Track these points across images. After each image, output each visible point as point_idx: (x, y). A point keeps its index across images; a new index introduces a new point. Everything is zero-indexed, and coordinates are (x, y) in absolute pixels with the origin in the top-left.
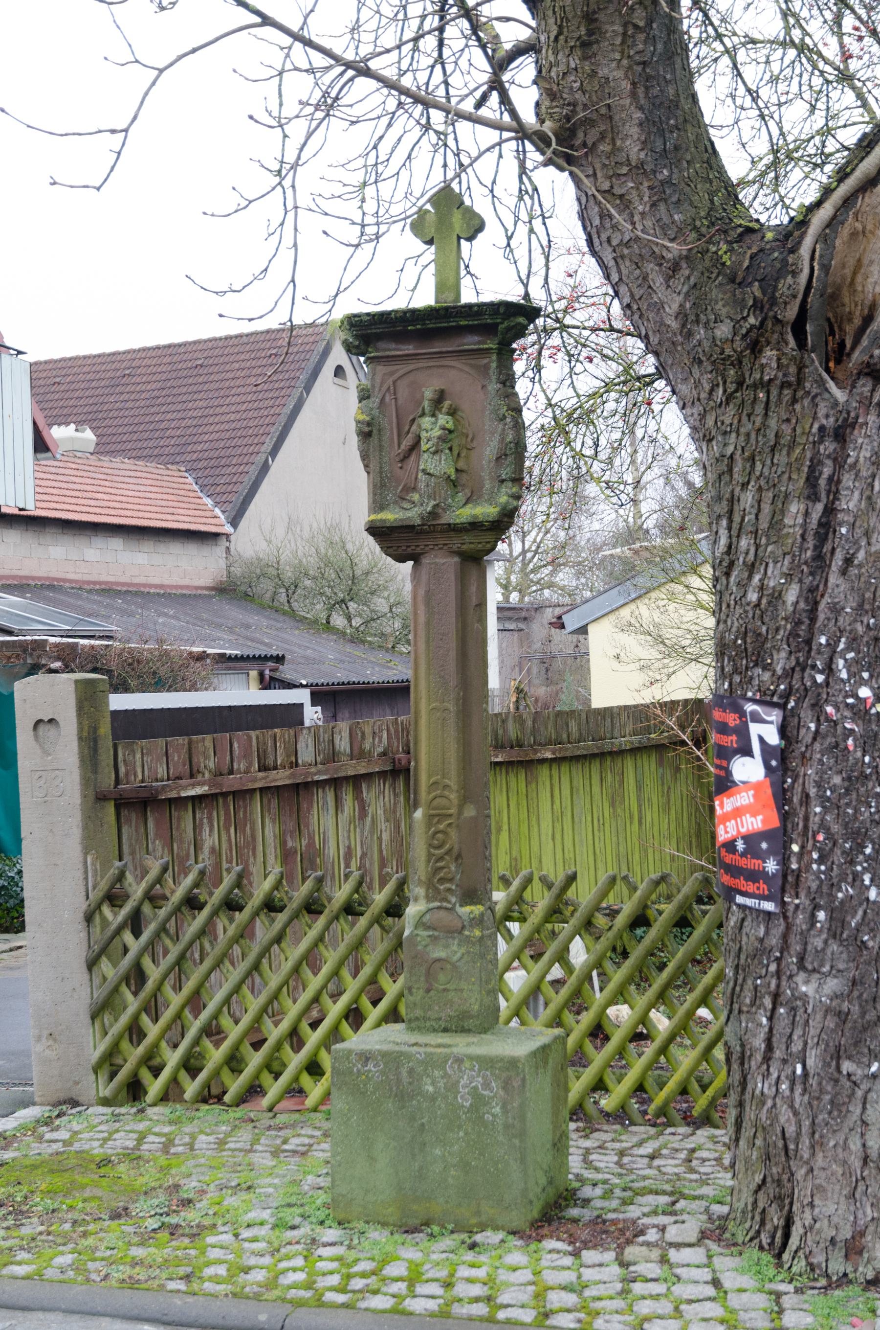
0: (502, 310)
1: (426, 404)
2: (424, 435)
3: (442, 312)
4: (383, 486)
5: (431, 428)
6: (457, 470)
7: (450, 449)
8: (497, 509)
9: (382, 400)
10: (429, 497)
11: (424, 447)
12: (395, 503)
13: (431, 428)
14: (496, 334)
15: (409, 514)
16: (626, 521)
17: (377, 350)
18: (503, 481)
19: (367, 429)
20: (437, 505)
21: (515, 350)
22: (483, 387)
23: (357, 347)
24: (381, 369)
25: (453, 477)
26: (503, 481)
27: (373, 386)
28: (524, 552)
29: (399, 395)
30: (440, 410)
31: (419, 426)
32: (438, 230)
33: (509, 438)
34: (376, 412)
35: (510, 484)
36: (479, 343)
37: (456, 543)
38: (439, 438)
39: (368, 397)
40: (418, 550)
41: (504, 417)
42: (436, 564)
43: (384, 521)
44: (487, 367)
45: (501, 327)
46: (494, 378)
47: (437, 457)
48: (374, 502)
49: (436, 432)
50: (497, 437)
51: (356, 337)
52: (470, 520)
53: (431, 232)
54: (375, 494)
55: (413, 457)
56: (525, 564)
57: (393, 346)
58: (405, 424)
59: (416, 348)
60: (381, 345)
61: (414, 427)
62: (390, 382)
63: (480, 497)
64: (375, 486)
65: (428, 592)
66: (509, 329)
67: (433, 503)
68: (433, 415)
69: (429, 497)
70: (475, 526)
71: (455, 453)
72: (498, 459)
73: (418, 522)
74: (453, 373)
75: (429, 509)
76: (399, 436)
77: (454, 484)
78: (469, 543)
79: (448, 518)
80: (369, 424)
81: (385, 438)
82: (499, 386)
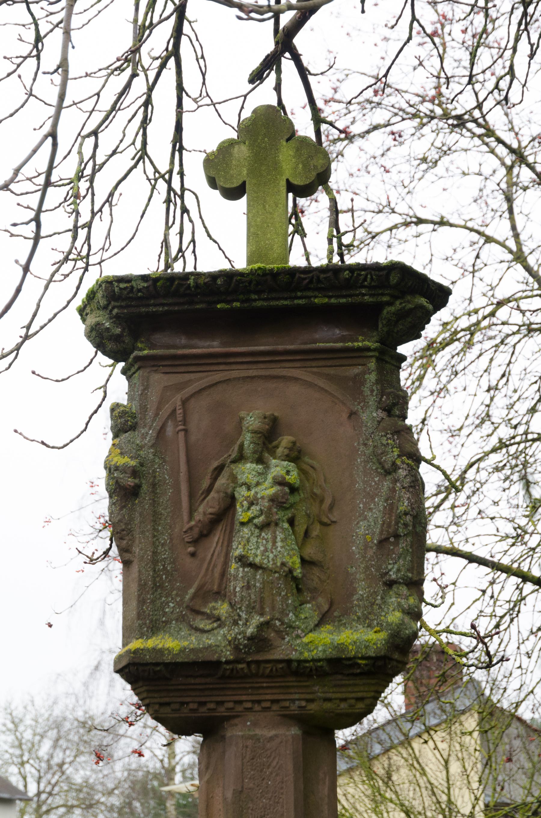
0: (394, 279)
1: (247, 439)
2: (242, 493)
3: (285, 279)
4: (157, 586)
5: (257, 482)
6: (303, 561)
7: (291, 522)
8: (383, 635)
9: (161, 432)
10: (251, 609)
11: (242, 515)
12: (181, 619)
13: (257, 482)
14: (375, 327)
15: (209, 640)
16: (162, 761)
17: (152, 347)
18: (390, 584)
19: (131, 482)
20: (267, 624)
21: (403, 358)
22: (352, 414)
23: (117, 338)
24: (159, 380)
25: (298, 572)
26: (390, 584)
27: (143, 408)
28: (39, 794)
29: (192, 426)
30: (273, 453)
31: (234, 478)
32: (253, 171)
33: (404, 506)
34: (148, 453)
35: (404, 590)
36: (343, 339)
37: (297, 700)
38: (273, 499)
39: (133, 428)
40: (222, 711)
41: (395, 468)
42: (256, 738)
43: (161, 652)
44: (358, 382)
45: (387, 311)
46: (372, 401)
47: (267, 535)
48: (140, 616)
49: (267, 490)
50: (380, 503)
51: (117, 319)
52: (331, 653)
53: (239, 174)
54: (141, 602)
55: (217, 537)
56: (39, 806)
57: (184, 341)
58: (207, 472)
59: (224, 345)
60: (159, 338)
61: (222, 481)
62: (177, 399)
63: (346, 612)
64: (142, 587)
65: (239, 793)
66: (402, 315)
67: (257, 620)
68: (260, 460)
69: (251, 609)
70: (339, 665)
71: (301, 529)
72: (382, 542)
73: (228, 654)
74: (293, 390)
75: (250, 631)
76: (191, 496)
77: (298, 585)
78: (319, 698)
79: (286, 649)
80: (135, 473)
81: (164, 500)
82: (381, 414)
